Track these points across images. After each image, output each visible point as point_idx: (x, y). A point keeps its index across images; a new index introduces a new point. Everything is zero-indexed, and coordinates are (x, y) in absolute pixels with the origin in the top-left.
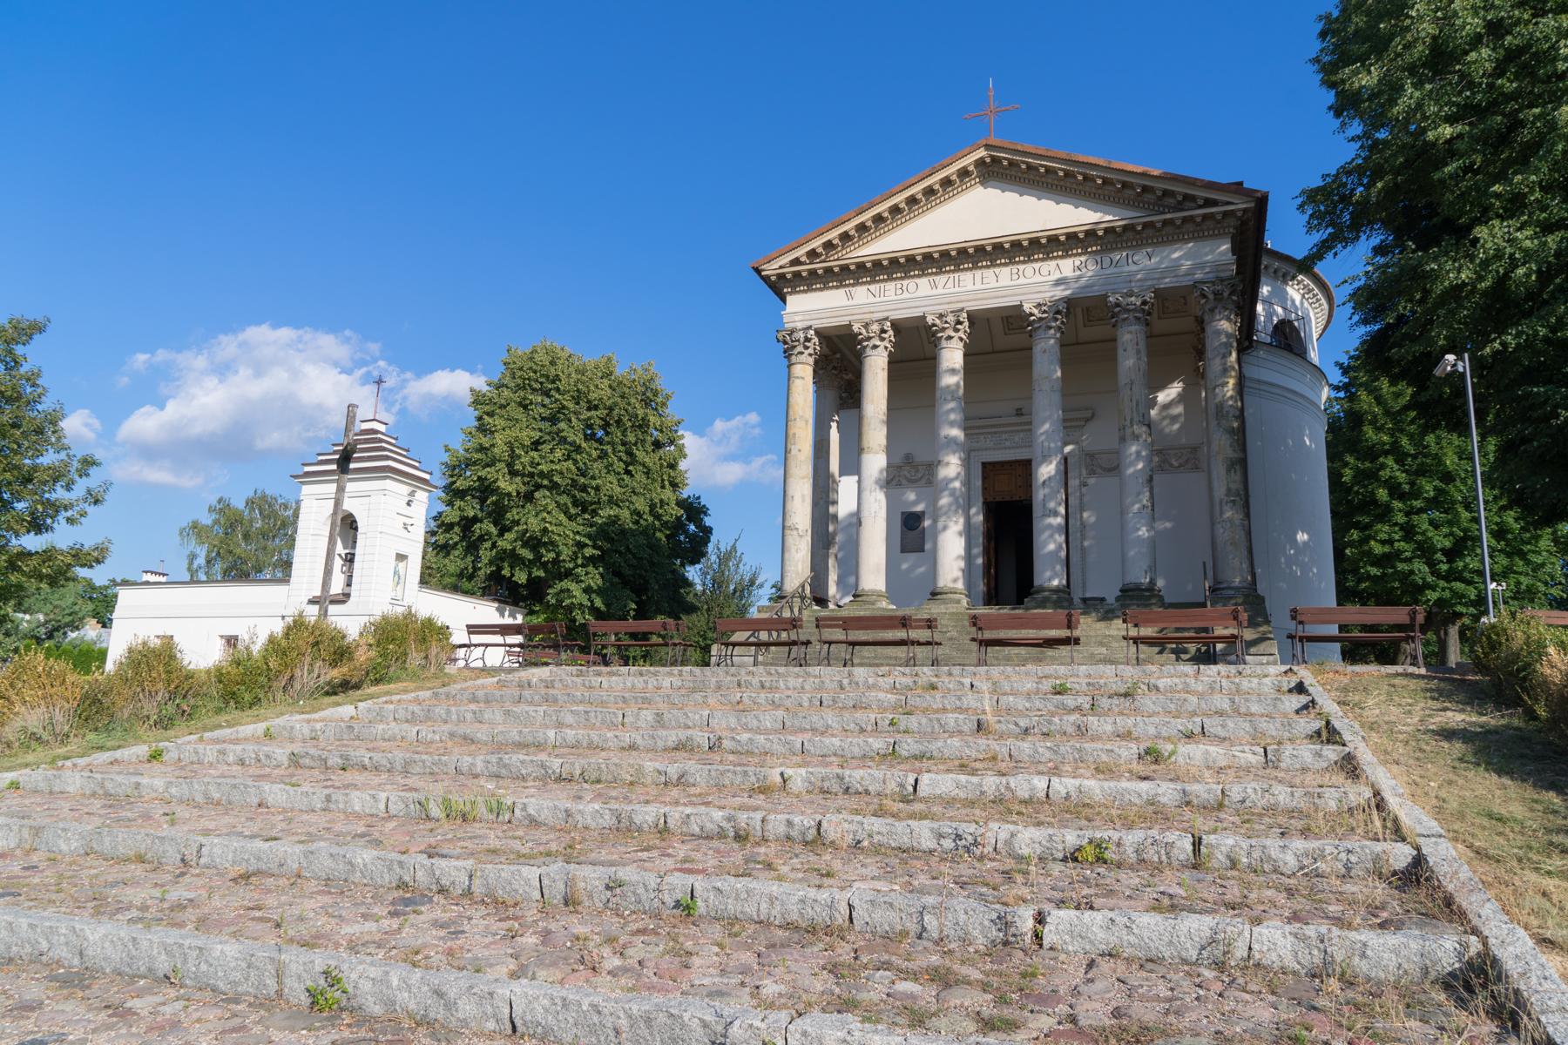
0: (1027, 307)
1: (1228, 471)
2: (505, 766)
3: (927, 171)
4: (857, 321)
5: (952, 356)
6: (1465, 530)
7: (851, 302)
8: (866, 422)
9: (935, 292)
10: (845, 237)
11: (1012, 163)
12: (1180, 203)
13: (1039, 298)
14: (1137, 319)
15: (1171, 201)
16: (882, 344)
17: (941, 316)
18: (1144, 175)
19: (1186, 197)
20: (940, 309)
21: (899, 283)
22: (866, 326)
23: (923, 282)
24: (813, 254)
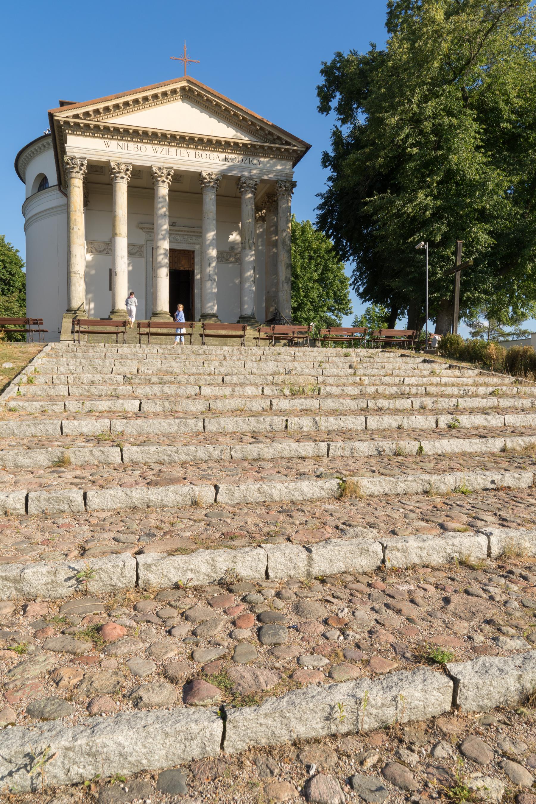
0: (204, 174)
1: (286, 269)
2: (248, 379)
3: (156, 84)
4: (114, 161)
5: (164, 190)
6: (301, 300)
7: (107, 149)
8: (117, 219)
9: (155, 154)
10: (107, 109)
11: (199, 94)
12: (274, 139)
13: (209, 171)
14: (253, 191)
15: (270, 137)
16: (126, 177)
17: (160, 169)
18: (261, 121)
19: (279, 138)
20: (161, 165)
21: (136, 144)
22: (118, 165)
23: (150, 147)
24: (87, 114)
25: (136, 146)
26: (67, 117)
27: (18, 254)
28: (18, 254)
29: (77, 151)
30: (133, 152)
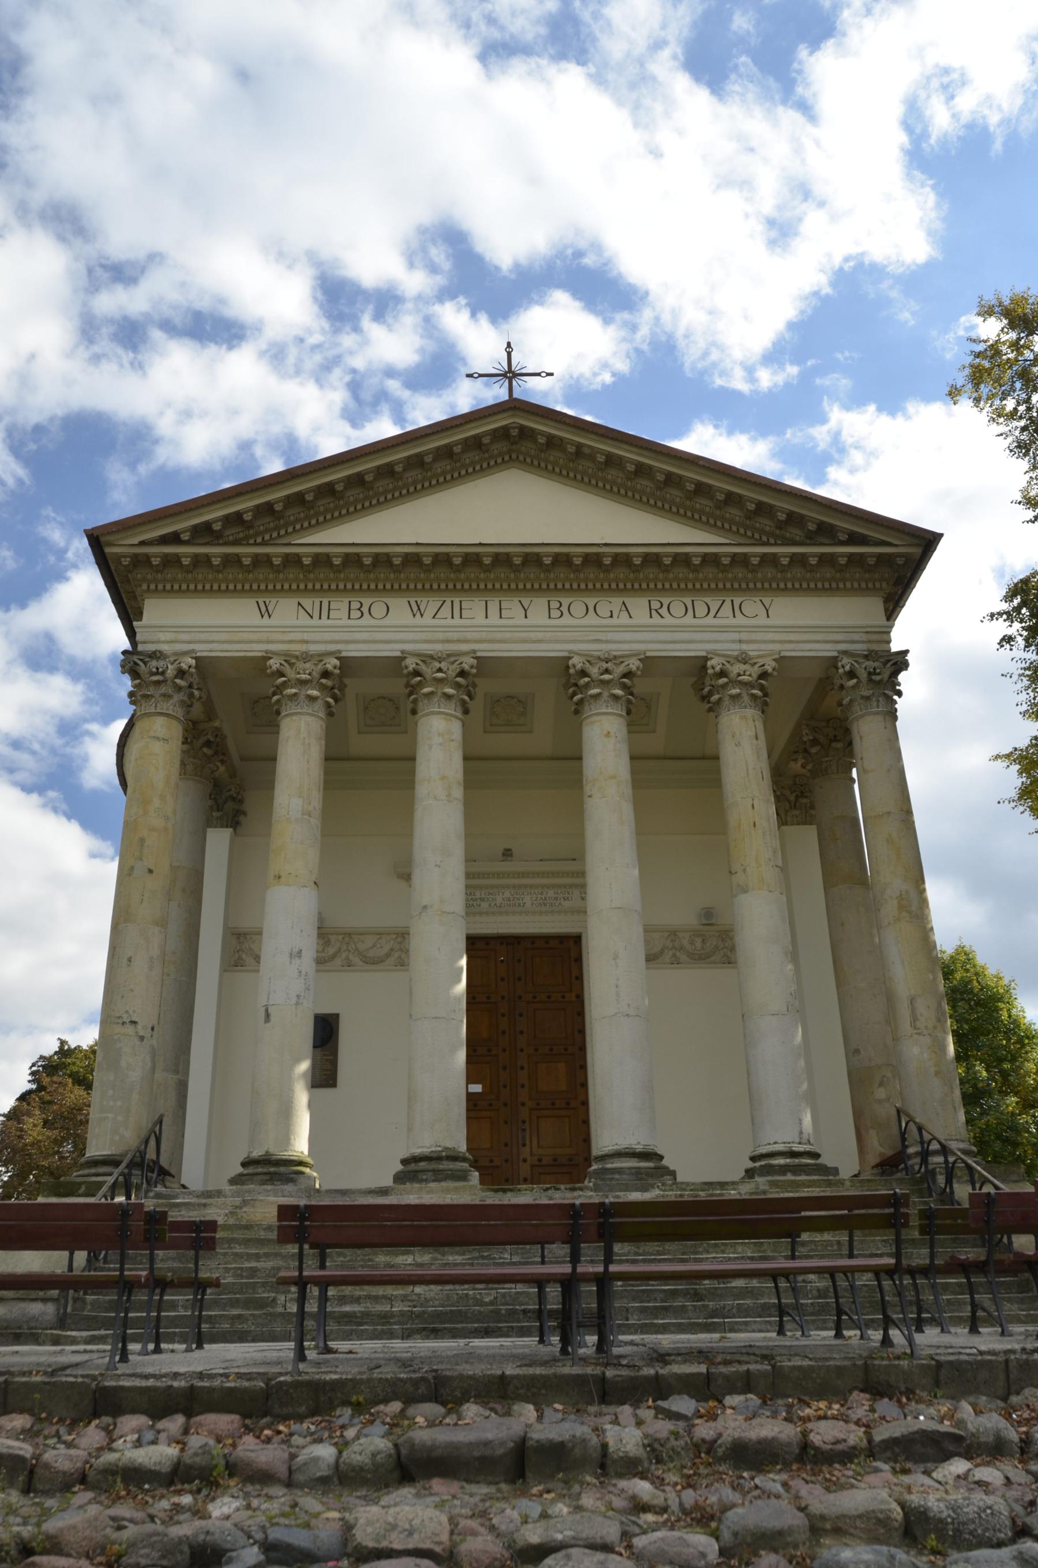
25: (355, 605)
26: (142, 543)
27: (939, 1330)
28: (939, 1330)
29: (169, 636)
30: (345, 622)
